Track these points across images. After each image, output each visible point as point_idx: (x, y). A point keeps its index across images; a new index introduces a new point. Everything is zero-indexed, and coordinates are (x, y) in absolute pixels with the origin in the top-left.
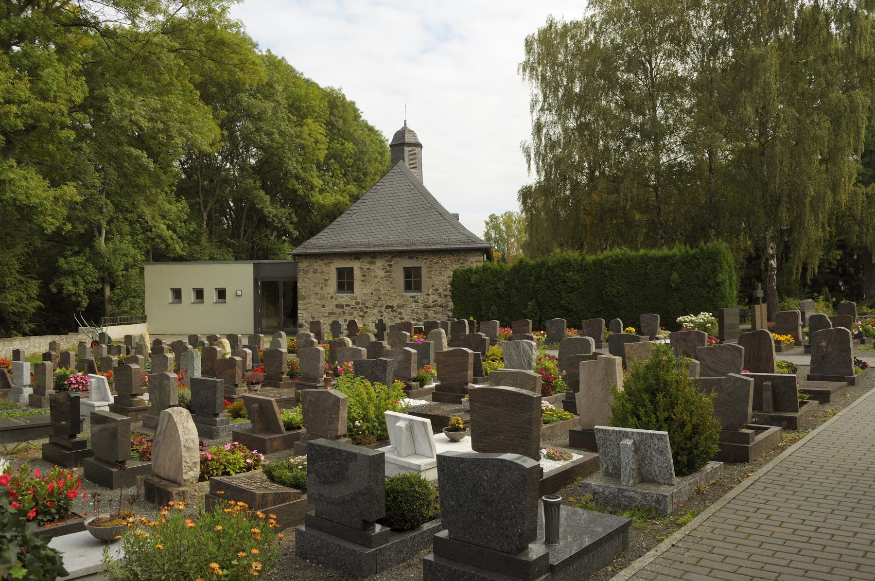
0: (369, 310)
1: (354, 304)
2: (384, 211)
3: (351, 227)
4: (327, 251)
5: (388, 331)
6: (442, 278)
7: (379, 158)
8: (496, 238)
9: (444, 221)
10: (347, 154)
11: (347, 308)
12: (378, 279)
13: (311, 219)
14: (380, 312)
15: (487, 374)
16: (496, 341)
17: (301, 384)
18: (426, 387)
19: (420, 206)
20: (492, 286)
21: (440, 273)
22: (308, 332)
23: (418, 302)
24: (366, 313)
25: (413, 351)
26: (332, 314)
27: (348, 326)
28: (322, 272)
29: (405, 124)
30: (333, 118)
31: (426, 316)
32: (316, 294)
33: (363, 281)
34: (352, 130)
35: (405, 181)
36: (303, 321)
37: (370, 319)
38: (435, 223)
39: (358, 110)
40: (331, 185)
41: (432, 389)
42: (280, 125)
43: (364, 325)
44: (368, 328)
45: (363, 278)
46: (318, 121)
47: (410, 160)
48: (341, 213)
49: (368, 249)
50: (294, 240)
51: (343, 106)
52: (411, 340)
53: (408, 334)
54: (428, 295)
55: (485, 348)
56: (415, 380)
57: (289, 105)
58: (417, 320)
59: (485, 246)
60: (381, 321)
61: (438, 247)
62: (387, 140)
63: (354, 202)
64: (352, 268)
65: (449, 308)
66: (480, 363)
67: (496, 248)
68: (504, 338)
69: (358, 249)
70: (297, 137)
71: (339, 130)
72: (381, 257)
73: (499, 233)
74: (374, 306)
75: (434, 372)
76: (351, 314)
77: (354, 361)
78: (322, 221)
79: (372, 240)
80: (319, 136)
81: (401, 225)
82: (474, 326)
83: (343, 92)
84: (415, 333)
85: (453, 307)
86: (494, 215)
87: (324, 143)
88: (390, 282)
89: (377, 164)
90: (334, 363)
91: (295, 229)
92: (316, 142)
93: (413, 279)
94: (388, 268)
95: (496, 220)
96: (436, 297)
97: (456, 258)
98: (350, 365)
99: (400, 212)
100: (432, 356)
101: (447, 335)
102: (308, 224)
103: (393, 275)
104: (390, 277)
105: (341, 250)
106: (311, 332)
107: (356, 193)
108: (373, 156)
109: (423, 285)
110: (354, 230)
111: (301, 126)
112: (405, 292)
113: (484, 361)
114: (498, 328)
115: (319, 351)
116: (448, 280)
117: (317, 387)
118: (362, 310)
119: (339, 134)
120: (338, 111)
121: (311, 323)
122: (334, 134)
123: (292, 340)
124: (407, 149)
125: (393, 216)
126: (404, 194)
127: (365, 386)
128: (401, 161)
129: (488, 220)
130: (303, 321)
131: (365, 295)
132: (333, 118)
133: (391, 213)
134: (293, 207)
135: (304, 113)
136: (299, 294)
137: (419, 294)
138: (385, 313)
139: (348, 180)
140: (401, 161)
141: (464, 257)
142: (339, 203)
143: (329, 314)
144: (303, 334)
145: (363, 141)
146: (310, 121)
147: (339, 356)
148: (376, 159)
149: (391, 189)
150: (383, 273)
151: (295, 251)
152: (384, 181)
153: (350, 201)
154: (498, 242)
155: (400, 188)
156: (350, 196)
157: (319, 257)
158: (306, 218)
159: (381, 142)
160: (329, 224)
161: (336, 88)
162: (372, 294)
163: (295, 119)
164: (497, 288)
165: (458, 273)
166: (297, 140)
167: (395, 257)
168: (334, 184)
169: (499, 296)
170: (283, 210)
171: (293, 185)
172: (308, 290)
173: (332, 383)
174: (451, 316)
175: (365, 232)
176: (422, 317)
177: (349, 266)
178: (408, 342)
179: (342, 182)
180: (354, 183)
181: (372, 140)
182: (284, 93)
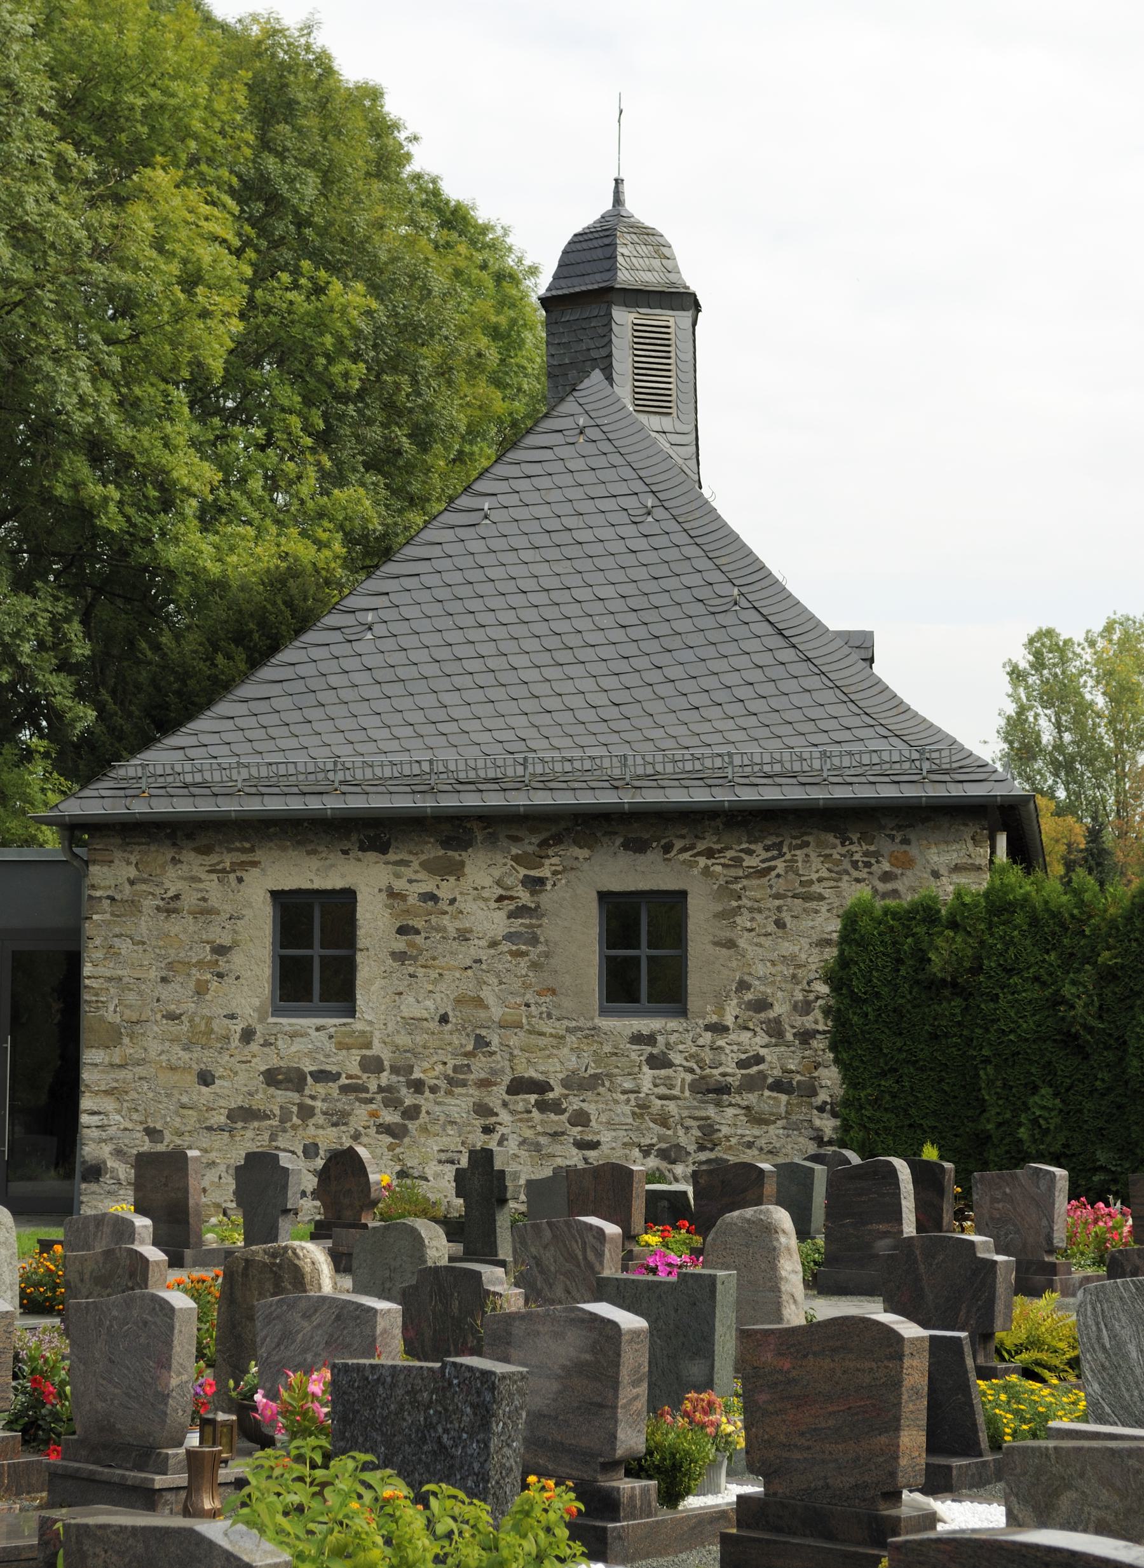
0: (426, 1101)
1: (354, 1067)
2: (508, 617)
3: (346, 694)
4: (229, 806)
5: (517, 1205)
6: (787, 948)
7: (493, 356)
8: (1059, 747)
9: (802, 668)
10: (340, 340)
11: (321, 1089)
12: (476, 949)
13: (157, 647)
14: (482, 1110)
15: (996, 1444)
16: (1052, 1269)
17: (73, 1476)
18: (693, 1502)
19: (683, 596)
20: (1033, 993)
21: (780, 924)
22: (123, 1208)
23: (669, 1064)
24: (412, 1113)
25: (629, 1321)
26: (244, 1115)
27: (323, 1175)
28: (205, 912)
29: (618, 200)
30: (271, 163)
31: (708, 1136)
32: (172, 1017)
33: (400, 957)
34: (361, 222)
35: (610, 475)
36: (106, 1150)
37: (433, 1146)
38: (755, 675)
39: (395, 126)
40: (256, 484)
41: (719, 1515)
42: (20, 199)
43: (402, 1174)
44: (423, 1188)
45: (400, 944)
46: (203, 180)
47: (639, 372)
48: (304, 622)
49: (427, 803)
50: (77, 747)
51: (323, 105)
52: (629, 1256)
53: (612, 1229)
54: (719, 1029)
55: (991, 1301)
56: (636, 1468)
57: (63, 103)
58: (664, 1155)
59: (999, 791)
60: (482, 1158)
61: (771, 794)
62: (533, 271)
63: (370, 570)
64: (348, 896)
65: (823, 1096)
66: (965, 1388)
67: (1061, 794)
68: (1091, 1254)
69: (379, 802)
70: (99, 254)
71: (302, 222)
72: (492, 841)
73: (1078, 723)
74: (451, 1081)
75: (732, 1426)
76: (339, 1119)
77: (334, 1367)
78: (210, 660)
79: (450, 755)
80: (206, 253)
81: (588, 685)
82: (940, 1191)
83: (321, 40)
84: (652, 1220)
85: (840, 1092)
86: (1050, 633)
87: (226, 283)
88: (535, 966)
89: (483, 388)
90: (239, 1371)
91: (79, 694)
92: (191, 280)
93: (644, 952)
94: (524, 897)
95: (1064, 661)
96: (757, 1042)
97: (858, 851)
98: (316, 1388)
99: (584, 624)
100: (726, 1345)
101: (803, 1234)
102: (144, 676)
103: (549, 930)
104: (534, 941)
105: (296, 804)
106: (140, 1210)
107: (376, 525)
108: (462, 345)
109: (695, 982)
110: (363, 708)
111: (120, 201)
112: (603, 1012)
113: (986, 1373)
114: (1061, 1202)
115: (167, 1309)
116: (818, 960)
117: (148, 1498)
118: (390, 1097)
119: (302, 239)
120: (299, 130)
121: (143, 1162)
122: (276, 244)
123: (46, 1246)
124: (624, 318)
125: (552, 642)
126: (607, 533)
127: (382, 1505)
128: (597, 375)
129: (1024, 660)
130: (106, 1150)
131: (412, 1024)
132: (271, 163)
133: (541, 628)
134: (73, 590)
135: (136, 141)
136: (89, 1014)
137: (673, 1024)
138: (504, 1116)
139: (338, 463)
140: (597, 375)
141: (897, 848)
142: (294, 572)
143: (232, 1115)
144: (100, 1220)
145: (413, 278)
146: (160, 178)
147: (265, 1335)
148: (476, 363)
149: (542, 511)
150: (500, 917)
151: (73, 808)
152: (513, 471)
153: (349, 563)
154: (1069, 767)
155: (586, 506)
156: (350, 540)
157: (190, 836)
158: (132, 643)
159: (504, 277)
160: (245, 677)
161: (291, 20)
162: (444, 1019)
163: (90, 166)
164: (1057, 1001)
165: (864, 923)
166: (100, 270)
167: (558, 840)
168: (273, 483)
169: (1069, 1040)
170: (26, 604)
171: (76, 486)
172: (131, 997)
173: (225, 1474)
174: (828, 1133)
175: (416, 717)
176: (687, 1140)
177: (333, 881)
178: (610, 1270)
179: (312, 473)
180: (372, 478)
181: (457, 273)
182: (41, 46)
